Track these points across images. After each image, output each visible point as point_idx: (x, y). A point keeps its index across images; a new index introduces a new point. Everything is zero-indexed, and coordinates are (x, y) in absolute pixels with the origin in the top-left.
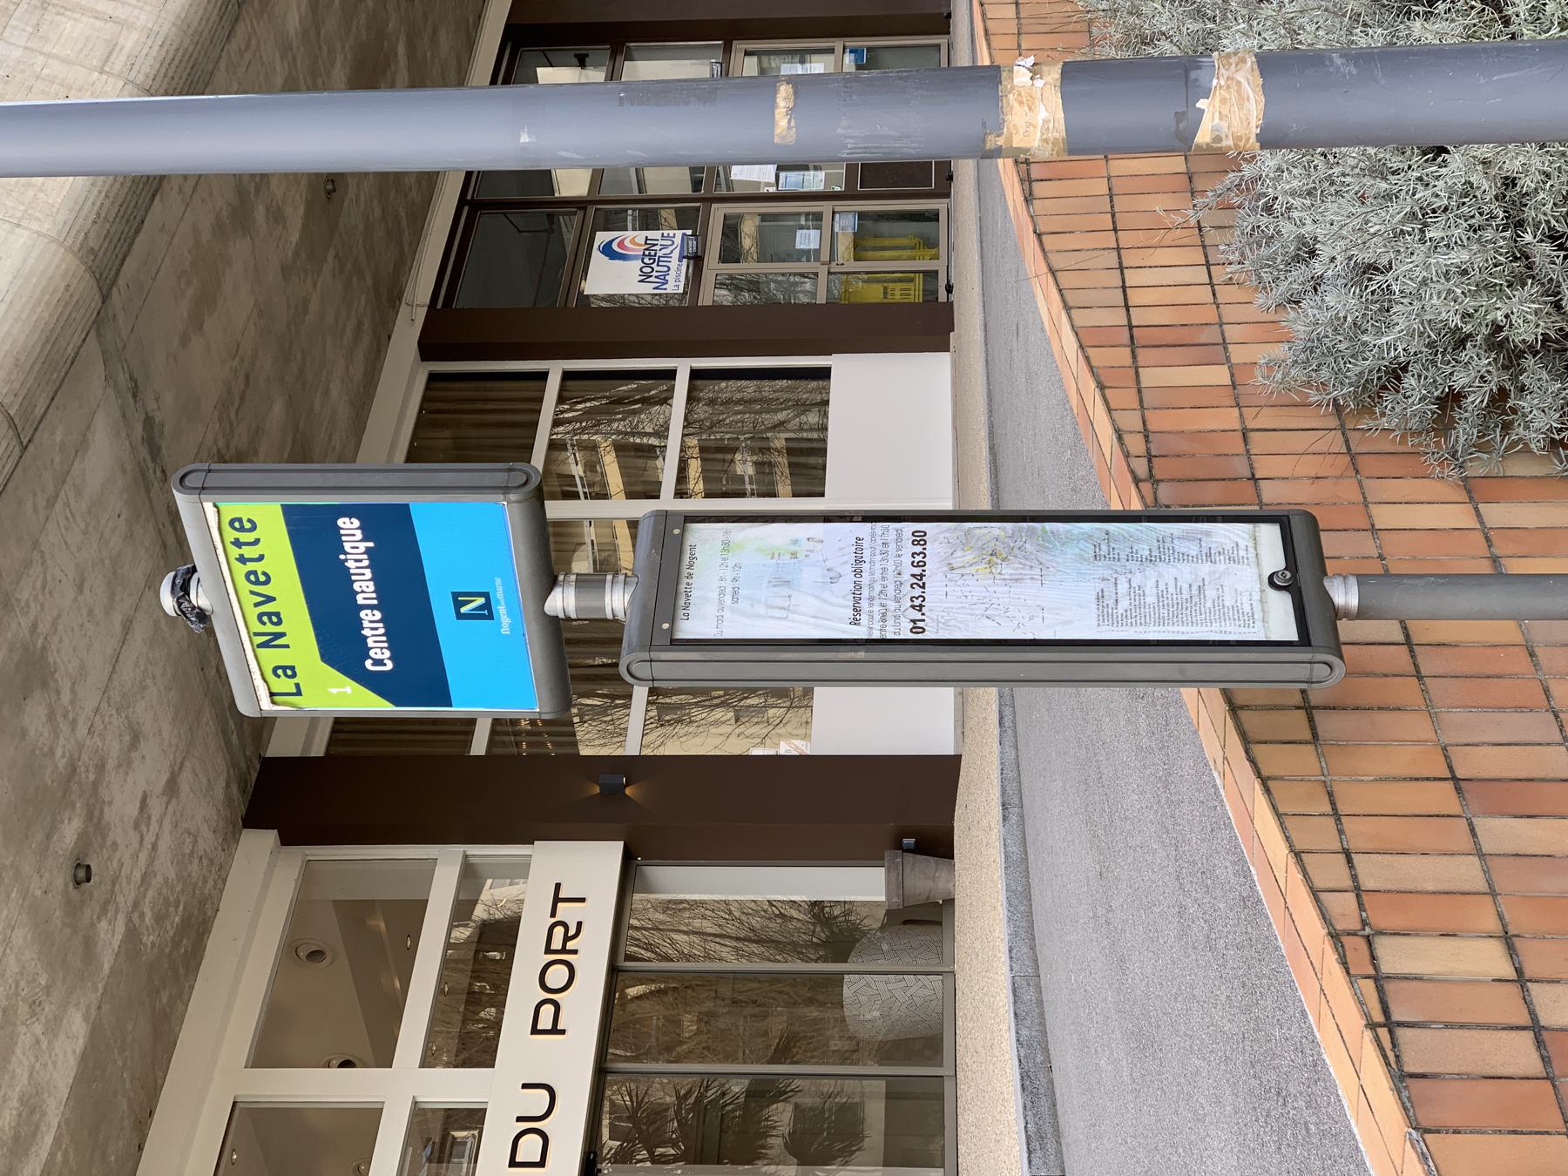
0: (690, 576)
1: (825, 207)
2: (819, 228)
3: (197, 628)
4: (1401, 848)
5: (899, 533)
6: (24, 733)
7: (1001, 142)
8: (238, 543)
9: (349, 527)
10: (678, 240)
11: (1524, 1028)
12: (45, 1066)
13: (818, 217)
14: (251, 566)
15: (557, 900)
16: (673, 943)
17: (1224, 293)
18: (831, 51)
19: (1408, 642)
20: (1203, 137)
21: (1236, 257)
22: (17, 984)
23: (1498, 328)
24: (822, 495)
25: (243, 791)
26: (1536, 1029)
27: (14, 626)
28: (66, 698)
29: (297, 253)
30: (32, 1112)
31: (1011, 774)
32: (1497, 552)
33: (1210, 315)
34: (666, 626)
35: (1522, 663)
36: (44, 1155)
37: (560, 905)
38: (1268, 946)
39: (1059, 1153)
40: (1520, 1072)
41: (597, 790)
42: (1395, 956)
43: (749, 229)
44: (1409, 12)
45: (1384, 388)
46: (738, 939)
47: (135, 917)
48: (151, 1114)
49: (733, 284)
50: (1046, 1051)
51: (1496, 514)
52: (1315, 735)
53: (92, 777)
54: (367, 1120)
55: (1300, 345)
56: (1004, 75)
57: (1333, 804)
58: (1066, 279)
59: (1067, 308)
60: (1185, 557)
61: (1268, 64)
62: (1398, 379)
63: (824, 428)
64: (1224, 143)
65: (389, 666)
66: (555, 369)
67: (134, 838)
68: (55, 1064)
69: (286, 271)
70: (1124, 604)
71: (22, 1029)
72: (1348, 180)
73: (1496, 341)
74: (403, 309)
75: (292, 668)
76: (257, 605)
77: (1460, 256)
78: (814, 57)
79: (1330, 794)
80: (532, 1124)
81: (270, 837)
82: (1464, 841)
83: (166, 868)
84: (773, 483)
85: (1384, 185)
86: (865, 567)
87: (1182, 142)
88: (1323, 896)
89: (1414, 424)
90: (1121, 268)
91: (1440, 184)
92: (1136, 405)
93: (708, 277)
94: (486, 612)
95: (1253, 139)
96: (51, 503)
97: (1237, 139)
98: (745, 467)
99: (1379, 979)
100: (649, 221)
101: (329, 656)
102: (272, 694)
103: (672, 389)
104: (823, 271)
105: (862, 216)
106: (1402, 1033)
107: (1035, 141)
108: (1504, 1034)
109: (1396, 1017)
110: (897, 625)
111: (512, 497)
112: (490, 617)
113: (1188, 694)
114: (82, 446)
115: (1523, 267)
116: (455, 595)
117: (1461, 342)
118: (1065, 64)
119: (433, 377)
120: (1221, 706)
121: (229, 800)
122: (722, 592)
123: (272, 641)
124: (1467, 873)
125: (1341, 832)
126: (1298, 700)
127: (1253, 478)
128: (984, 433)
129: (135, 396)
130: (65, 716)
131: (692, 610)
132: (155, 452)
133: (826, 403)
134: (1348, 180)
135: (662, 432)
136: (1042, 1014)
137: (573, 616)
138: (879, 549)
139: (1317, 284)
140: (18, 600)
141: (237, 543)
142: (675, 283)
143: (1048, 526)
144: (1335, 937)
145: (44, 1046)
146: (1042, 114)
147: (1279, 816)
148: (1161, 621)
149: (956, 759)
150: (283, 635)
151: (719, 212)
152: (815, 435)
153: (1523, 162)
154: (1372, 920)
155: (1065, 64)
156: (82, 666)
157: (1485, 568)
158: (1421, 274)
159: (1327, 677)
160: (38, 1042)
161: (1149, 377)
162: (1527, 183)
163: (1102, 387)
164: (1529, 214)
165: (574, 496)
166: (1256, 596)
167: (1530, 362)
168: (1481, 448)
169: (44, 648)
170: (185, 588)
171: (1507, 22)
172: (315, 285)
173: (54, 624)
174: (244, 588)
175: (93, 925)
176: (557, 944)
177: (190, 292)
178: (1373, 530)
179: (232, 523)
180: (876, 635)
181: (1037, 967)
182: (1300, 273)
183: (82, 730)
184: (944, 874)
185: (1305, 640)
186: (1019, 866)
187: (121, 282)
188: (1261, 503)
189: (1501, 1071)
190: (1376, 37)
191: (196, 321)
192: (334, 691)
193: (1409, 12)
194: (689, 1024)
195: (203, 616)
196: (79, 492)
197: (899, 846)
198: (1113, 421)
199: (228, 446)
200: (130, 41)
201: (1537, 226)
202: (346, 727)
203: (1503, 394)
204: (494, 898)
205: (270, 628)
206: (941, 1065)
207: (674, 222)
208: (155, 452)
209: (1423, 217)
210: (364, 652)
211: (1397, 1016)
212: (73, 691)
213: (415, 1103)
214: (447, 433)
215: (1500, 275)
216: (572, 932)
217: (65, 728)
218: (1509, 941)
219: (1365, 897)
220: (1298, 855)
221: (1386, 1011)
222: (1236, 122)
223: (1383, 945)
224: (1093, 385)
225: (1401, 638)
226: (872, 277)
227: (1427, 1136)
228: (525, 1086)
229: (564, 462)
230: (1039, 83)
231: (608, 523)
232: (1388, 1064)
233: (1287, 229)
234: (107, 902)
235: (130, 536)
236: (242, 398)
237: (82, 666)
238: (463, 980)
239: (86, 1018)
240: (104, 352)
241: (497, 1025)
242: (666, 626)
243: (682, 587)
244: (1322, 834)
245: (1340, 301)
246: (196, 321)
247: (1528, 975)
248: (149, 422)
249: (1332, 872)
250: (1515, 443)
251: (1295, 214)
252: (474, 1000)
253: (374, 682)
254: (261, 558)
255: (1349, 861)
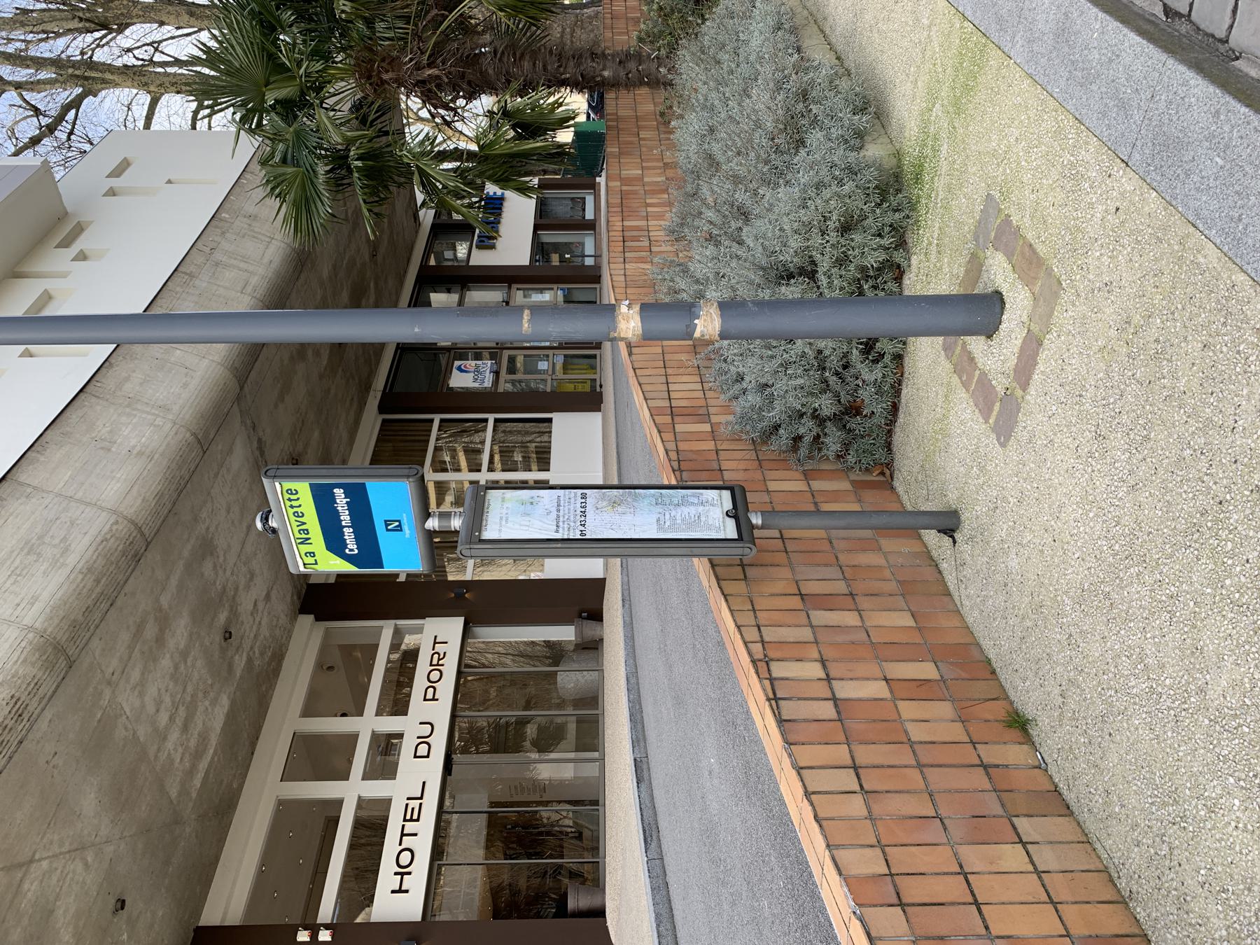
0: (488, 512)
1: (550, 352)
2: (548, 360)
3: (271, 536)
4: (780, 624)
5: (576, 494)
6: (202, 575)
7: (616, 335)
8: (290, 500)
9: (339, 492)
10: (489, 365)
11: (830, 699)
12: (210, 720)
13: (548, 356)
14: (295, 509)
15: (435, 643)
16: (486, 658)
17: (709, 394)
18: (552, 289)
19: (782, 537)
20: (697, 334)
21: (713, 380)
22: (198, 683)
23: (816, 410)
24: (549, 470)
25: (299, 598)
26: (835, 699)
27: (199, 528)
28: (221, 559)
29: (325, 369)
30: (204, 740)
31: (626, 587)
32: (817, 500)
33: (702, 403)
34: (477, 534)
35: (826, 546)
36: (209, 759)
37: (437, 645)
38: (728, 663)
39: (645, 747)
40: (828, 718)
41: (453, 595)
42: (778, 670)
43: (520, 361)
44: (780, 283)
45: (771, 433)
46: (513, 655)
47: (251, 653)
48: (257, 739)
49: (513, 382)
50: (640, 704)
51: (817, 485)
52: (745, 576)
53: (232, 593)
54: (353, 738)
55: (738, 415)
56: (617, 308)
57: (753, 605)
58: (646, 388)
59: (646, 399)
60: (693, 504)
61: (723, 306)
62: (777, 430)
63: (550, 442)
64: (705, 337)
65: (356, 551)
66: (437, 418)
67: (251, 619)
68: (214, 718)
69: (321, 377)
70: (668, 524)
71: (200, 704)
72: (756, 350)
73: (815, 415)
74: (372, 393)
75: (313, 553)
76: (298, 526)
77: (800, 381)
78: (547, 291)
79: (752, 601)
80: (423, 739)
81: (312, 617)
82: (805, 621)
83: (265, 632)
84: (530, 466)
85: (770, 352)
86: (561, 508)
87: (689, 335)
88: (749, 645)
89: (784, 448)
90: (667, 383)
91: (792, 352)
92: (673, 439)
93: (502, 380)
94: (399, 528)
95: (717, 336)
96: (216, 475)
97: (711, 336)
98: (518, 457)
99: (772, 680)
100: (478, 357)
101: (330, 547)
102: (304, 564)
103: (486, 426)
104: (549, 378)
105: (565, 356)
106: (782, 703)
107: (630, 335)
108: (822, 702)
109: (778, 696)
110: (574, 533)
111: (411, 480)
112: (401, 530)
113: (695, 560)
114: (230, 451)
115: (825, 387)
116: (386, 521)
117: (802, 415)
118: (642, 304)
119: (384, 421)
120: (709, 565)
121: (293, 602)
122: (501, 518)
123: (305, 541)
124: (806, 634)
125: (756, 617)
126: (739, 562)
127: (720, 470)
128: (614, 446)
129: (254, 429)
130: (221, 567)
131: (488, 527)
132: (262, 453)
133: (551, 432)
134: (756, 350)
135: (483, 442)
136: (639, 688)
137: (437, 529)
138: (567, 500)
139: (744, 392)
140: (201, 518)
141: (290, 500)
142: (488, 383)
143: (637, 491)
144: (754, 662)
145: (210, 710)
146: (632, 324)
147: (731, 611)
148: (683, 531)
149: (604, 579)
150: (309, 539)
151: (506, 353)
152: (547, 444)
153: (826, 345)
154: (769, 654)
155: (642, 304)
156: (229, 546)
157: (813, 509)
158: (785, 388)
159: (750, 553)
160: (207, 709)
161: (679, 428)
162: (827, 353)
163: (659, 432)
164: (827, 365)
165: (445, 470)
166: (721, 520)
167: (828, 424)
168: (809, 458)
169: (212, 538)
170: (267, 519)
171: (818, 287)
172: (333, 382)
173: (217, 528)
174: (293, 518)
175: (232, 657)
176: (435, 662)
177: (279, 385)
178: (768, 491)
179: (287, 491)
180: (566, 537)
181: (636, 669)
182: (737, 387)
183: (228, 573)
184: (599, 628)
185: (740, 538)
186: (629, 626)
187: (249, 381)
188: (723, 481)
189: (821, 718)
190: (766, 295)
191: (281, 398)
192: (332, 562)
193: (780, 283)
194: (493, 693)
195: (274, 531)
196: (228, 470)
197: (580, 616)
198: (664, 446)
199: (294, 450)
200: (254, 280)
201: (831, 369)
202: (340, 576)
203: (817, 437)
204: (409, 641)
205: (304, 536)
206: (597, 709)
207: (488, 356)
208: (262, 453)
209: (786, 365)
210: (345, 546)
211: (779, 696)
212: (224, 555)
213: (373, 731)
214: (391, 444)
215: (817, 389)
216: (441, 657)
217: (220, 572)
218: (823, 663)
219: (766, 645)
220: (738, 627)
221: (774, 693)
222: (710, 328)
223: (774, 665)
224: (656, 431)
225: (779, 536)
226: (571, 381)
227: (792, 747)
228: (421, 723)
229: (442, 456)
230: (631, 312)
231: (461, 482)
232: (775, 716)
233: (732, 368)
234: (238, 648)
235: (251, 490)
236: (301, 430)
237: (229, 546)
238: (395, 677)
239: (228, 698)
240: (241, 411)
241: (409, 695)
242: (477, 534)
243: (484, 518)
244: (748, 619)
245: (754, 399)
246: (281, 398)
247: (831, 677)
248: (260, 441)
249: (752, 634)
250: (823, 456)
251: (735, 363)
252: (400, 685)
253: (349, 559)
254: (300, 506)
255: (759, 629)
